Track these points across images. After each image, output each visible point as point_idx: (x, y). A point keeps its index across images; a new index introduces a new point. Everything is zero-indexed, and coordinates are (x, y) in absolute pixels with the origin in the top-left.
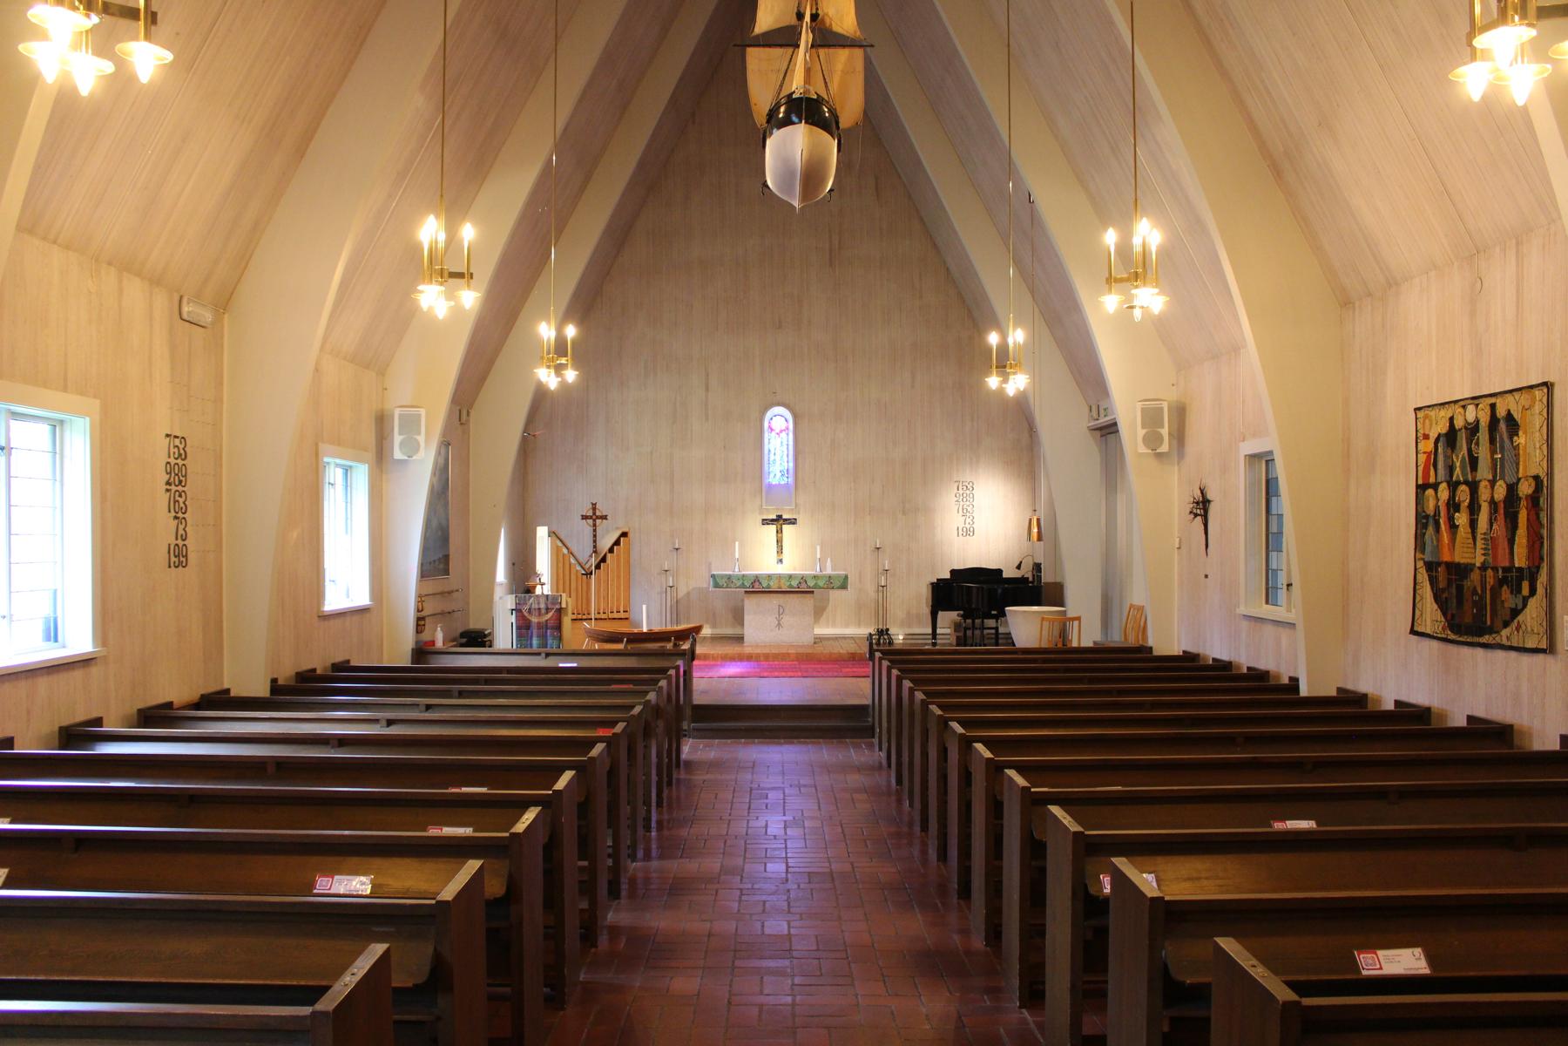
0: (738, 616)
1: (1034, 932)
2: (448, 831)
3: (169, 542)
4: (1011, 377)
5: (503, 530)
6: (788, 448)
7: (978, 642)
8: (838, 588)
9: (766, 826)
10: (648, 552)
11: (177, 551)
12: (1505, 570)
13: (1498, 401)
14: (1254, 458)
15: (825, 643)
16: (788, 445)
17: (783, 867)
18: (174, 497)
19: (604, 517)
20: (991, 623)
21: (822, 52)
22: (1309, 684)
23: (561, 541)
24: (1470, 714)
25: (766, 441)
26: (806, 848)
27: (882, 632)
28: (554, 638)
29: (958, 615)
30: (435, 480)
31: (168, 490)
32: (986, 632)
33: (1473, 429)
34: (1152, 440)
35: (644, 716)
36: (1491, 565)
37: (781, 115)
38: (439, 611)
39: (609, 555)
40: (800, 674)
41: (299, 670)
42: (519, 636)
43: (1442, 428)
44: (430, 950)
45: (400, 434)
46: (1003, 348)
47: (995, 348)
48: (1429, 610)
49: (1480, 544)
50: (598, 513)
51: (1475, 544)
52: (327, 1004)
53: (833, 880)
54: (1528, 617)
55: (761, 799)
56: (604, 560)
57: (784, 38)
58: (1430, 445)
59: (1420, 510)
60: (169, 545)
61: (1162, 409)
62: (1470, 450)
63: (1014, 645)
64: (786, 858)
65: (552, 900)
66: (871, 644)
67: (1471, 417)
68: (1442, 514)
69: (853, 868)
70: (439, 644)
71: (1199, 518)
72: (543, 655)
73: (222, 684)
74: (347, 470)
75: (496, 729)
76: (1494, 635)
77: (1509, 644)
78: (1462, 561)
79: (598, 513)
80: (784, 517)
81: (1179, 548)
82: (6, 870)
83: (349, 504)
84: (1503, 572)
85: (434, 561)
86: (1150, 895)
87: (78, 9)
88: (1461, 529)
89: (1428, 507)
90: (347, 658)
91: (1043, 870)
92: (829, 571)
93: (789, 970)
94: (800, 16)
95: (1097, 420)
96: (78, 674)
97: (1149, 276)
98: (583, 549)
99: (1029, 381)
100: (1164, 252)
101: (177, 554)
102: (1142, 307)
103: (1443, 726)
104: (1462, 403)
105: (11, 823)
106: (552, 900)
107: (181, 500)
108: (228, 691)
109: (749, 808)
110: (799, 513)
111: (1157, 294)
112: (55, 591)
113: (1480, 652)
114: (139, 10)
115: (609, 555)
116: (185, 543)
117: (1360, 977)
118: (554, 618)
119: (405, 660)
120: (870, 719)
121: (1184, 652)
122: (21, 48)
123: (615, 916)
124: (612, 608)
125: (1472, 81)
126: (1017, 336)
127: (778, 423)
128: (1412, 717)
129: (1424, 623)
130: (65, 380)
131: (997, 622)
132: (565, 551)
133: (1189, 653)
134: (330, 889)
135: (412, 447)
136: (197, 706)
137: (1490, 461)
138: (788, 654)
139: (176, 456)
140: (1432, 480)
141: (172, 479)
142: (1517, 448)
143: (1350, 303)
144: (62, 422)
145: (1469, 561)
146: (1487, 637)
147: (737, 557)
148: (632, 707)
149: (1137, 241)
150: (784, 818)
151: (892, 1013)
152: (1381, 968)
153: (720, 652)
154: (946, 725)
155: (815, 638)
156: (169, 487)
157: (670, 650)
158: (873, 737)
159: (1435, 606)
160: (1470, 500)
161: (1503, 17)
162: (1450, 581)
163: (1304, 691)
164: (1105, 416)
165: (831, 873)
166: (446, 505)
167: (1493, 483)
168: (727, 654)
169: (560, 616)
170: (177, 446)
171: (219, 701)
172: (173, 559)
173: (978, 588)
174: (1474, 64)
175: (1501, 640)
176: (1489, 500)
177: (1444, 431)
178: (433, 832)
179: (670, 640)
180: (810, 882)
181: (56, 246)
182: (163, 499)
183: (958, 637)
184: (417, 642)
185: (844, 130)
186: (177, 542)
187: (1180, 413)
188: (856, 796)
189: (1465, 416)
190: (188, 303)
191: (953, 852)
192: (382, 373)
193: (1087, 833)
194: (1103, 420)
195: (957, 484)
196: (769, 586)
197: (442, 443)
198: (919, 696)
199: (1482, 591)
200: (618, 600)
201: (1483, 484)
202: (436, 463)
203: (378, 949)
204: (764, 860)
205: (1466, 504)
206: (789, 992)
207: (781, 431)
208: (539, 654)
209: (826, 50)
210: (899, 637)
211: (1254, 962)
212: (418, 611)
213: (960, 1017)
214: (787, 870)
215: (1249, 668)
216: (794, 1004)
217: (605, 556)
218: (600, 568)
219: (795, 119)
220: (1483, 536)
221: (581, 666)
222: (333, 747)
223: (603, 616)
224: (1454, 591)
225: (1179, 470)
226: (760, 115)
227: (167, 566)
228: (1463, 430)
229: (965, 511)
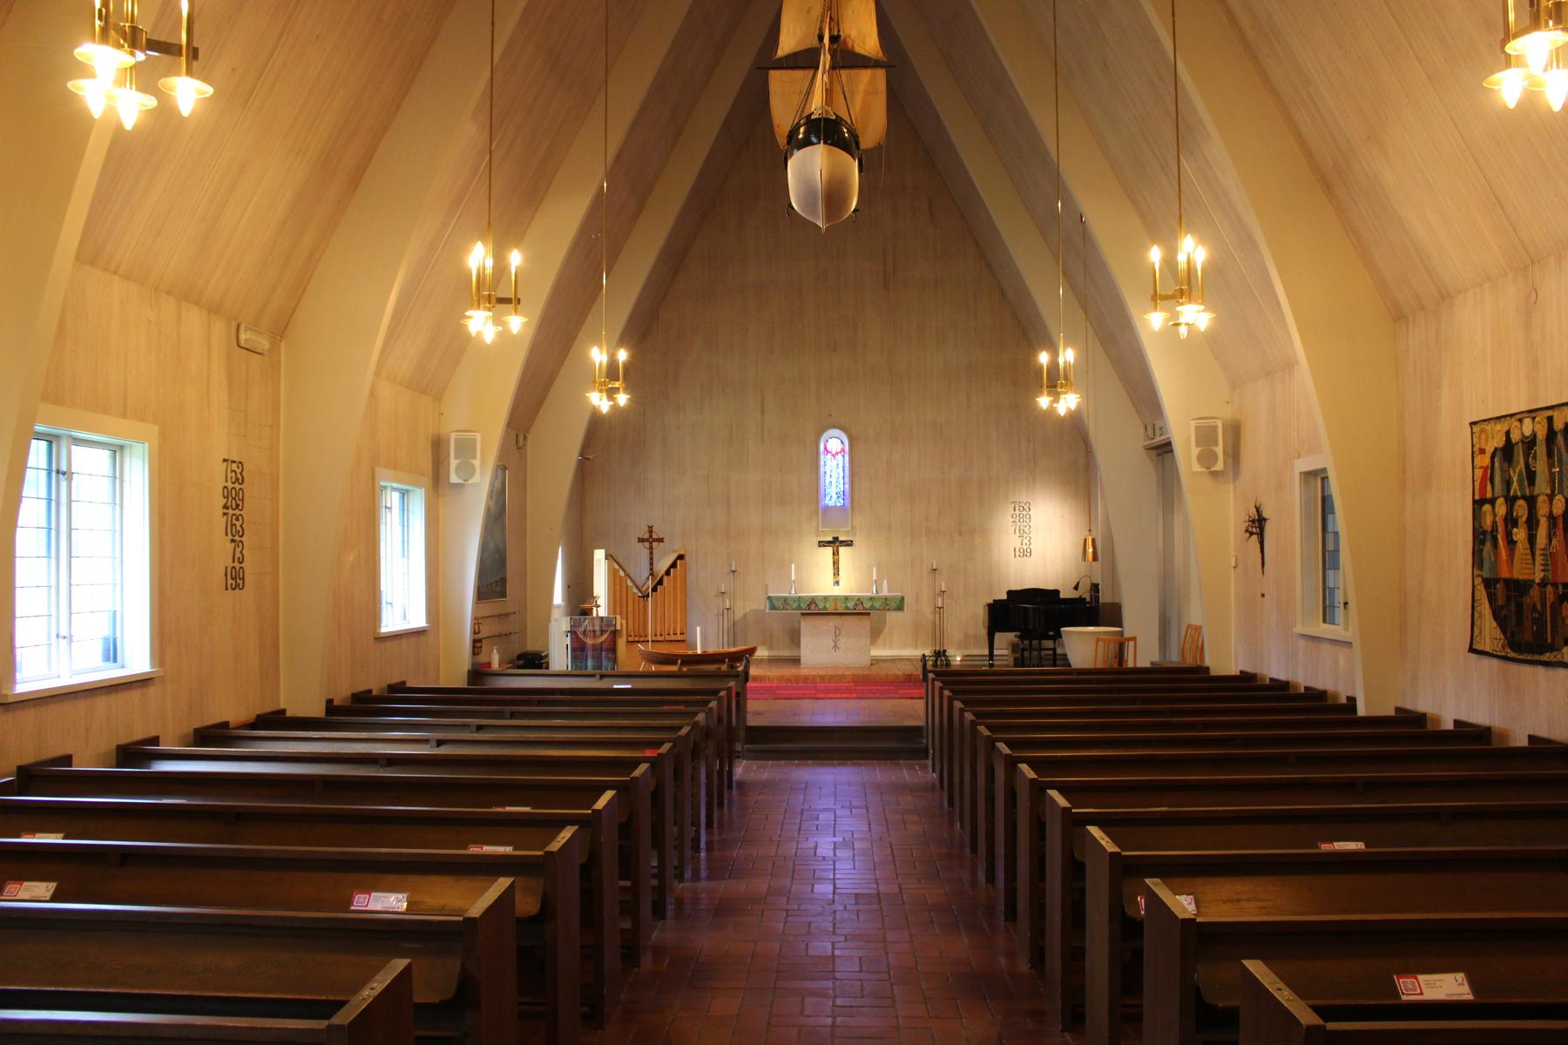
0: (795, 638)
1: (1075, 956)
2: (488, 849)
4: (1062, 396)
5: (560, 549)
6: (844, 470)
7: (1036, 662)
9: (816, 848)
10: (705, 575)
11: (234, 573)
13: (1555, 414)
14: (1309, 475)
15: (881, 664)
16: (844, 467)
17: (831, 888)
18: (232, 521)
19: (661, 540)
20: (1048, 644)
21: (844, 73)
22: (1367, 706)
23: (618, 563)
24: (1531, 733)
25: (822, 463)
26: (854, 869)
27: (939, 654)
28: (609, 659)
29: (1015, 636)
30: (492, 504)
31: (225, 514)
32: (1043, 653)
33: (1530, 443)
34: (1207, 458)
35: (692, 737)
36: (1551, 582)
37: (801, 136)
38: (497, 634)
39: (666, 578)
40: (855, 695)
41: (355, 691)
42: (574, 658)
43: (1499, 442)
44: (458, 967)
45: (456, 458)
48: (1487, 627)
49: (1539, 559)
50: (654, 536)
51: (1534, 559)
52: (343, 1018)
53: (880, 902)
55: (811, 820)
56: (660, 582)
57: (805, 60)
58: (1486, 460)
59: (1477, 525)
60: (226, 568)
61: (1215, 428)
62: (1527, 465)
63: (1069, 665)
64: (834, 879)
65: (591, 917)
66: (925, 666)
67: (1527, 430)
68: (1500, 530)
69: (901, 890)
70: (495, 665)
71: (1255, 537)
72: (598, 676)
73: (278, 703)
74: (404, 494)
75: (545, 749)
76: (1556, 653)
78: (1521, 577)
79: (654, 536)
80: (841, 539)
81: (1235, 567)
82: (54, 884)
83: (406, 528)
85: (492, 583)
86: (1181, 916)
87: (123, 47)
88: (1519, 545)
89: (1485, 523)
90: (404, 679)
91: (1083, 892)
92: (885, 592)
93: (831, 992)
94: (821, 38)
95: (1153, 439)
96: (136, 694)
97: (1194, 293)
98: (641, 573)
99: (1080, 400)
100: (1212, 268)
101: (234, 576)
102: (1187, 324)
103: (1505, 746)
104: (1518, 417)
105: (64, 838)
106: (591, 917)
107: (238, 524)
108: (284, 711)
109: (799, 830)
110: (855, 535)
111: (1203, 311)
112: (115, 612)
113: (1540, 670)
114: (181, 47)
115: (666, 578)
116: (242, 565)
117: (1399, 1002)
118: (609, 639)
120: (924, 741)
121: (1241, 672)
122: (70, 85)
123: (662, 933)
124: (669, 630)
125: (1508, 87)
126: (1067, 356)
128: (1471, 737)
129: (1483, 641)
131: (1055, 642)
132: (622, 573)
133: (1247, 673)
134: (367, 906)
135: (467, 471)
136: (253, 725)
137: (1547, 474)
138: (844, 675)
140: (1489, 495)
141: (229, 503)
143: (1403, 317)
144: (122, 447)
145: (1527, 577)
146: (1548, 655)
147: (793, 579)
148: (680, 728)
149: (1182, 259)
150: (834, 839)
151: (932, 1036)
152: (1421, 993)
153: (776, 674)
154: (994, 746)
155: (872, 660)
156: (226, 511)
157: (723, 672)
158: (927, 758)
159: (1494, 624)
160: (1529, 515)
161: (1535, 23)
162: (1508, 599)
163: (1362, 711)
164: (1161, 435)
165: (878, 894)
166: (503, 529)
167: (1551, 497)
168: (783, 676)
169: (615, 637)
170: (235, 471)
171: (275, 721)
172: (230, 581)
173: (1035, 608)
174: (1508, 71)
175: (1563, 658)
176: (1547, 514)
177: (1500, 445)
178: (474, 850)
179: (724, 662)
180: (856, 904)
181: (116, 277)
182: (220, 522)
183: (1015, 659)
184: (473, 665)
185: (867, 151)
187: (1235, 431)
188: (907, 817)
189: (1521, 429)
190: (246, 331)
191: (1000, 875)
192: (438, 398)
193: (1123, 853)
194: (1159, 439)
195: (1013, 505)
196: (825, 608)
197: (498, 466)
198: (969, 716)
199: (1542, 607)
200: (675, 622)
201: (1541, 499)
202: (492, 485)
203: (401, 964)
204: (812, 881)
205: (1524, 519)
206: (830, 1014)
207: (837, 453)
208: (593, 676)
209: (848, 71)
210: (957, 659)
211: (1281, 985)
212: (475, 633)
213: (1001, 1041)
214: (834, 891)
215: (1306, 688)
216: (833, 1025)
218: (656, 591)
219: (814, 140)
220: (1541, 552)
222: (382, 766)
223: (659, 638)
224: (1513, 608)
225: (1235, 489)
226: (782, 141)
227: (224, 587)
228: (1520, 444)
229: (1022, 532)
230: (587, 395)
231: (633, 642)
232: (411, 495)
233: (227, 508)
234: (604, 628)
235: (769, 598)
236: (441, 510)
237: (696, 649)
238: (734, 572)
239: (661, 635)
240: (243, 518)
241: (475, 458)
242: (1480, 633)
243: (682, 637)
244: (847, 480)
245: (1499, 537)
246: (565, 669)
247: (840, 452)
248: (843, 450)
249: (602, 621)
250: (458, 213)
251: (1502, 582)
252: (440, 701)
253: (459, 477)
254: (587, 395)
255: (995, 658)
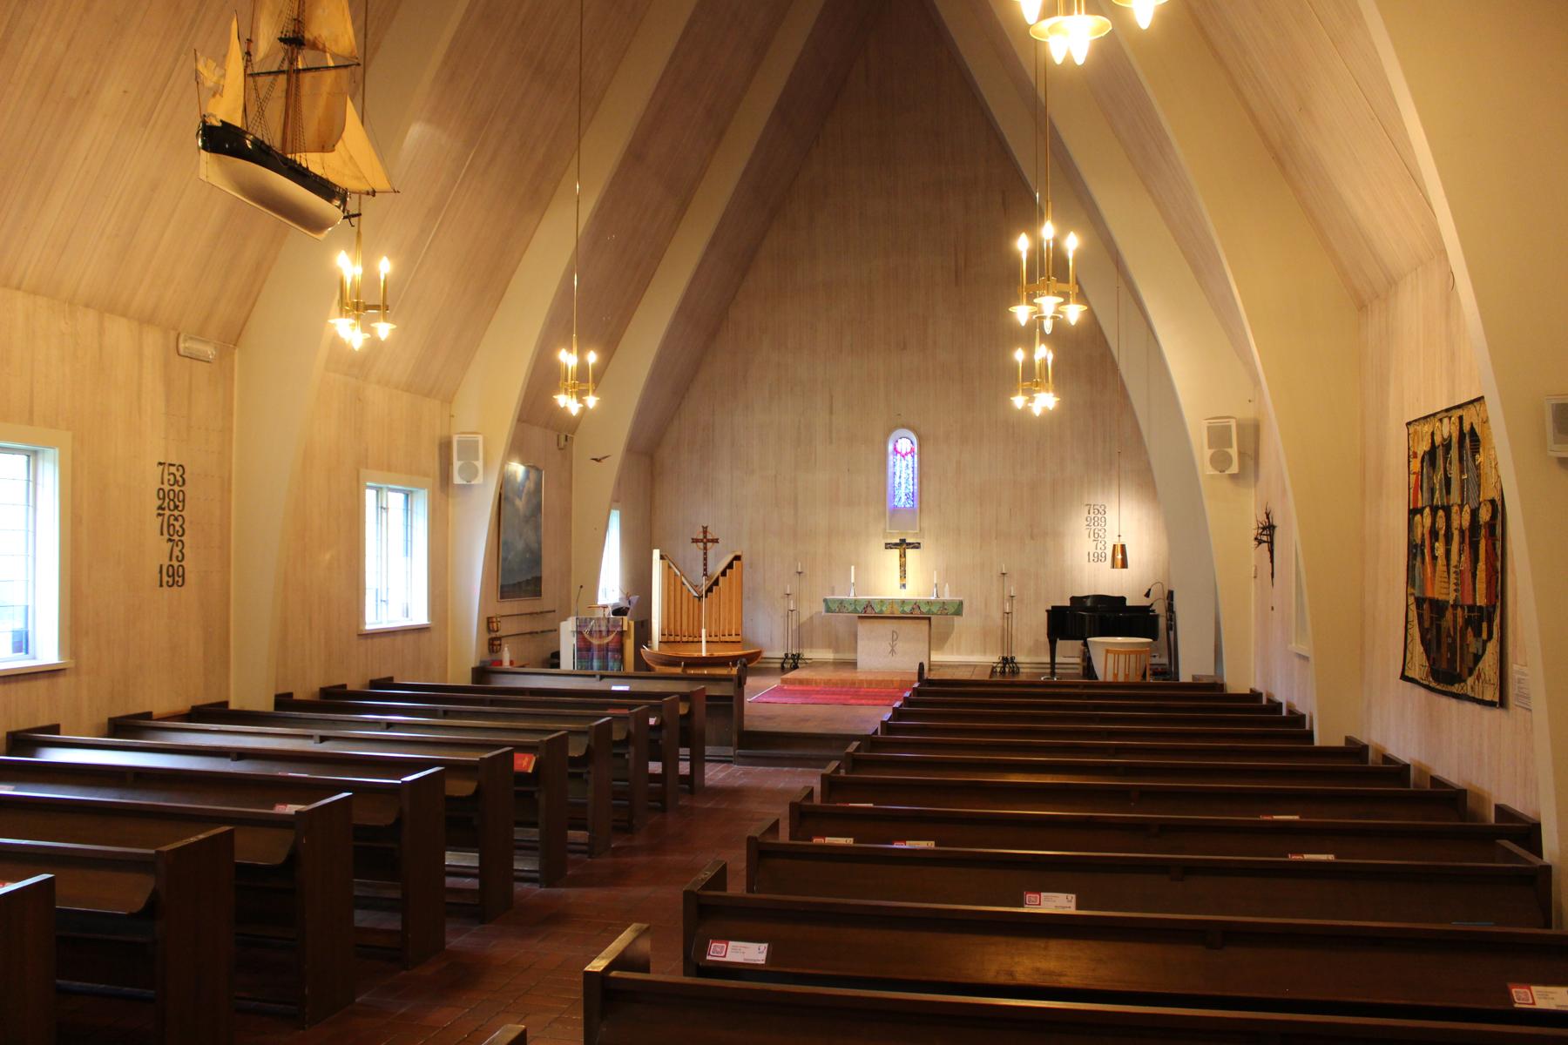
3: (161, 563)
6: (913, 471)
8: (952, 614)
12: (1469, 607)
19: (715, 541)
25: (891, 463)
28: (615, 660)
33: (1447, 446)
34: (1220, 461)
38: (528, 631)
39: (721, 579)
43: (1424, 447)
45: (459, 459)
46: (1029, 365)
47: (1021, 365)
48: (1417, 650)
49: (1453, 576)
54: (1487, 665)
56: (716, 583)
61: (1229, 427)
70: (506, 664)
72: (598, 677)
77: (1472, 695)
79: (709, 537)
80: (908, 541)
84: (1468, 612)
92: (946, 597)
96: (42, 685)
101: (171, 573)
112: (27, 607)
115: (721, 579)
118: (615, 640)
119: (465, 680)
124: (723, 631)
127: (904, 445)
130: (31, 412)
135: (470, 472)
138: (892, 681)
139: (172, 482)
141: (166, 505)
142: (1478, 467)
147: (853, 581)
162: (1432, 624)
167: (1461, 506)
172: (165, 578)
173: (1089, 616)
181: (20, 294)
186: (171, 563)
195: (1087, 508)
196: (881, 612)
200: (730, 623)
201: (1455, 509)
207: (906, 454)
217: (717, 580)
220: (1454, 569)
221: (633, 690)
227: (159, 583)
228: (1441, 447)
229: (1096, 536)
230: (555, 397)
231: (687, 642)
232: (414, 495)
233: (164, 509)
234: (611, 629)
235: (825, 600)
236: (450, 508)
237: (701, 651)
238: (800, 573)
239: (716, 636)
240: (183, 518)
241: (477, 459)
242: (1412, 658)
243: (738, 638)
244: (916, 480)
245: (1426, 551)
246: (572, 668)
247: (910, 453)
248: (912, 450)
249: (608, 622)
250: (440, 220)
251: (1427, 602)
252: (437, 697)
253: (462, 478)
254: (555, 397)
255: (1056, 666)
